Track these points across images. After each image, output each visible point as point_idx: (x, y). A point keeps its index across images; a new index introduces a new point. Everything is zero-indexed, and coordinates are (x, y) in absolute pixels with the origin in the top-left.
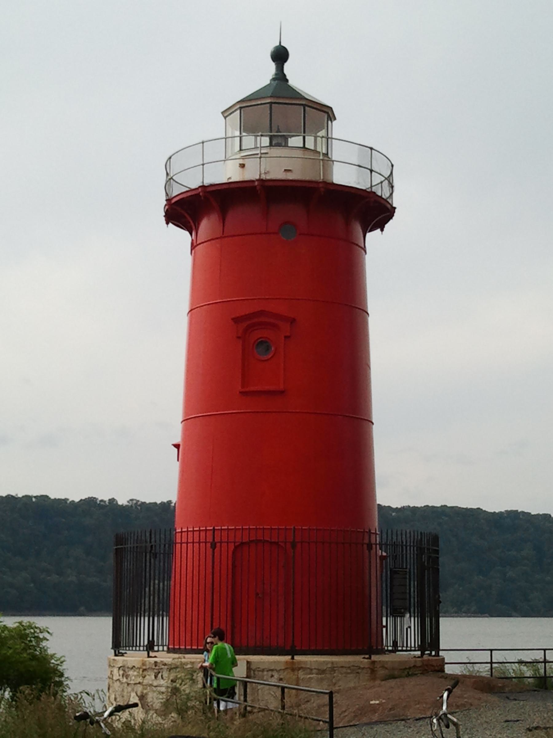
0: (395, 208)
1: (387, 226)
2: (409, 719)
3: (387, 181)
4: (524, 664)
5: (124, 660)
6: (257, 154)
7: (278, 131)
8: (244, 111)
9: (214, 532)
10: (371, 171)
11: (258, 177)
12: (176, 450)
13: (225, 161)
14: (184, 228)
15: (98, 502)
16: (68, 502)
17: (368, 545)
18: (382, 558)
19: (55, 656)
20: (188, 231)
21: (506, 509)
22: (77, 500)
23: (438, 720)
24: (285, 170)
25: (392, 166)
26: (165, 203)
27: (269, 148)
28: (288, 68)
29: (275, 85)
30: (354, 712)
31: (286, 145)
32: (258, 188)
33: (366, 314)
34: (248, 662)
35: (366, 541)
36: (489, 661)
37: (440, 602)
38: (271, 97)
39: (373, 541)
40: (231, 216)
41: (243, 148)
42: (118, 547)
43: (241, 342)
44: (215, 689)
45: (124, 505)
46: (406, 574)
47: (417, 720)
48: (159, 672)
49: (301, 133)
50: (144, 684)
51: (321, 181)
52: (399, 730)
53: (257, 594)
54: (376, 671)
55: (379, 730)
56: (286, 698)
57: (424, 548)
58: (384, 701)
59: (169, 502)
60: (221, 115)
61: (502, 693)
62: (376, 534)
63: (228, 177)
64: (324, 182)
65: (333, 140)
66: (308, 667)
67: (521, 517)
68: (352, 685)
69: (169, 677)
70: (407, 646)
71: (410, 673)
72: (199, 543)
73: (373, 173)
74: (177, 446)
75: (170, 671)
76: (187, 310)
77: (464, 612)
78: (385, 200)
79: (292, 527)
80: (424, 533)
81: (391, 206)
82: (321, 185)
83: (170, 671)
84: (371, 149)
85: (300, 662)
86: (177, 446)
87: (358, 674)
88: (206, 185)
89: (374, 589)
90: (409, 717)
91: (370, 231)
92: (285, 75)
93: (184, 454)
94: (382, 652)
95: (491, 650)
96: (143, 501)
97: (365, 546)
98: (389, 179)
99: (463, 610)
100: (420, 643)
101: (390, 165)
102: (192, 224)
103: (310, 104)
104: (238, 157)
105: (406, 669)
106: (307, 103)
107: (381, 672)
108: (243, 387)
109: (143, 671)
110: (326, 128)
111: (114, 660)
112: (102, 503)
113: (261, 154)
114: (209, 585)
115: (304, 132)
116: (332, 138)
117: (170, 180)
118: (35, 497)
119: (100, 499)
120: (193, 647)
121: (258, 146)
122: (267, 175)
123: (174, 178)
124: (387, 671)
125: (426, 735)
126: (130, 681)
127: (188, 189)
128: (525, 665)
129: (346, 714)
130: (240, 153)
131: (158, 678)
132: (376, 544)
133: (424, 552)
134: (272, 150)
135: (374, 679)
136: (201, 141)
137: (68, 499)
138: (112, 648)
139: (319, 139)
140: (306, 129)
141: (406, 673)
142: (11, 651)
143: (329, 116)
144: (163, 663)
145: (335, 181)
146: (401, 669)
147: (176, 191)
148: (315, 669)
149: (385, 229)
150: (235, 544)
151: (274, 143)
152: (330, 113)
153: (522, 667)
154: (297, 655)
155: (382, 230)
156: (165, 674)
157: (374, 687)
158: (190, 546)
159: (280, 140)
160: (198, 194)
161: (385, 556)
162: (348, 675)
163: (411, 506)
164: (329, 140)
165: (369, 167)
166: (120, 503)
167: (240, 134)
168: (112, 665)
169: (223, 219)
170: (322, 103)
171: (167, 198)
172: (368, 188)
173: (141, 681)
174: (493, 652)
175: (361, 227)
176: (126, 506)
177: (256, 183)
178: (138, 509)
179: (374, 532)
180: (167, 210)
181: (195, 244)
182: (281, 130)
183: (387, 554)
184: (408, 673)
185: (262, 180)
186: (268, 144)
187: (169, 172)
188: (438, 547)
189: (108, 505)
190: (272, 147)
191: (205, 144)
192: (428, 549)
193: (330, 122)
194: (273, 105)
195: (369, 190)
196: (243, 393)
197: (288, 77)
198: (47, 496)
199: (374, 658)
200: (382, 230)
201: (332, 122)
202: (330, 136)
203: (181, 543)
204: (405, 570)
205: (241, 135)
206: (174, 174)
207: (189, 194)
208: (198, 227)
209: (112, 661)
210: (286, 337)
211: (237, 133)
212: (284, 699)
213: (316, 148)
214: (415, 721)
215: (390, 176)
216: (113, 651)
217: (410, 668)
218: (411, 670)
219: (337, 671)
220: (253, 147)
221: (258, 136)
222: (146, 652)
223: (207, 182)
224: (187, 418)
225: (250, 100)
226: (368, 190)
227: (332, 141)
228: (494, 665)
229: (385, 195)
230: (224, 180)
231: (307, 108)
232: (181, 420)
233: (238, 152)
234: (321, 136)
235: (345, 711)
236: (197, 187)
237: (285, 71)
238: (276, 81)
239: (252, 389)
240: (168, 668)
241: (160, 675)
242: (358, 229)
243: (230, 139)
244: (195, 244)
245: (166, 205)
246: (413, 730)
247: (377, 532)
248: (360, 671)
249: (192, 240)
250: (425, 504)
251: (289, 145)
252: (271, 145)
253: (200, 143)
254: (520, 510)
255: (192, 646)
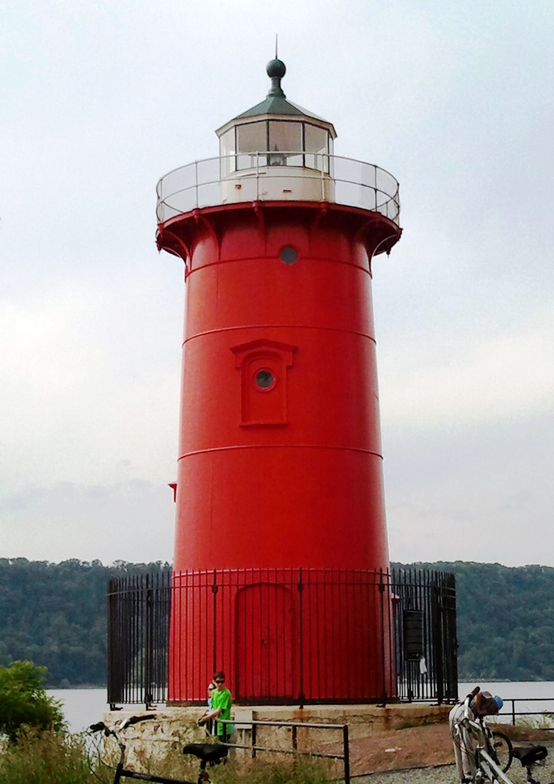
0: (402, 229)
1: (393, 249)
2: (427, 767)
3: (392, 201)
4: (549, 715)
5: (121, 715)
6: (255, 174)
7: (276, 150)
8: (239, 129)
9: (215, 576)
10: (376, 190)
11: (256, 199)
12: (173, 490)
13: (220, 181)
14: (178, 254)
15: (81, 564)
16: (48, 564)
17: (379, 585)
18: (395, 601)
19: (53, 699)
20: (182, 257)
21: (527, 564)
22: (58, 562)
23: (459, 726)
24: (284, 191)
25: (398, 185)
26: (156, 227)
27: (266, 167)
28: (285, 82)
29: (271, 101)
30: (369, 761)
31: (285, 165)
32: (256, 210)
33: (373, 342)
34: (254, 713)
35: (378, 582)
36: (511, 712)
37: (458, 646)
38: (268, 113)
39: (385, 582)
40: (226, 242)
41: (239, 168)
42: (112, 594)
43: (240, 373)
44: (220, 736)
45: (109, 567)
46: (421, 616)
47: (435, 767)
48: (159, 726)
49: (300, 151)
50: (143, 738)
51: (323, 201)
52: (417, 777)
53: (263, 641)
54: (391, 719)
55: (395, 778)
56: (297, 736)
57: (440, 589)
58: (400, 749)
59: (158, 563)
60: (215, 134)
61: (524, 741)
62: (388, 575)
63: (224, 199)
64: (327, 203)
65: (335, 158)
66: (318, 716)
67: (543, 571)
68: (365, 735)
69: (169, 730)
70: (423, 696)
71: (427, 721)
72: (200, 586)
73: (377, 192)
74: (174, 486)
75: (170, 724)
76: (182, 341)
77: (483, 677)
78: (392, 221)
79: (298, 569)
80: (439, 572)
81: (398, 226)
82: (323, 206)
83: (170, 724)
84: (376, 166)
85: (309, 712)
86: (174, 486)
87: (371, 724)
88: (201, 208)
89: (386, 635)
90: (427, 765)
91: (375, 255)
92: (282, 91)
93: (181, 497)
94: (396, 700)
95: (513, 700)
96: (130, 562)
97: (377, 586)
98: (395, 199)
99: (482, 675)
100: (436, 690)
101: (396, 184)
102: (187, 250)
103: (310, 121)
104: (234, 177)
105: (421, 717)
106: (307, 121)
107: (396, 721)
108: (244, 419)
109: (142, 725)
110: (327, 146)
111: (110, 714)
112: (85, 565)
113: (259, 174)
114: (211, 632)
115: (304, 150)
116: (334, 156)
117: (161, 202)
118: (11, 560)
119: (83, 560)
120: (195, 699)
121: (255, 165)
122: (266, 196)
123: (165, 201)
124: (402, 720)
125: (445, 781)
126: (128, 736)
127: (181, 213)
128: (550, 717)
129: (360, 762)
130: (236, 174)
131: (157, 732)
132: (388, 585)
133: (440, 593)
134: (270, 169)
135: (388, 728)
136: (194, 161)
137: (47, 562)
138: (108, 702)
139: (319, 157)
140: (306, 147)
141: (423, 722)
142: (9, 692)
143: (329, 133)
144: (163, 716)
145: (338, 202)
146: (416, 718)
147: (168, 215)
148: (325, 718)
149: (391, 252)
150: (238, 587)
151: (271, 162)
152: (331, 131)
153: (547, 718)
154: (306, 704)
155: (388, 253)
156: (166, 727)
157: (388, 735)
158: (190, 590)
159: (278, 160)
160: (193, 217)
161: (397, 599)
162: (361, 725)
163: (423, 562)
164: (331, 158)
165: (374, 187)
166: (105, 565)
167: (236, 153)
168: (108, 720)
169: (219, 243)
170: (323, 120)
171: (159, 222)
172: (373, 209)
173: (140, 736)
174: (515, 702)
175: (366, 248)
176: (112, 567)
177: (254, 205)
178: (125, 571)
179: (386, 573)
180: (159, 235)
181: (189, 271)
182: (278, 149)
183: (400, 596)
184: (425, 721)
185: (260, 201)
186: (266, 164)
187: (160, 195)
188: (454, 588)
189: (92, 568)
190: (270, 167)
191: (199, 164)
192: (444, 590)
193: (330, 139)
194: (270, 122)
195: (374, 211)
196: (244, 428)
197: (285, 93)
198: (25, 559)
199: (388, 706)
200: (388, 253)
201: (333, 139)
202: (331, 154)
203: (180, 587)
204: (420, 612)
205: (236, 155)
206: (166, 197)
207: (184, 217)
208: (192, 254)
209: (108, 715)
210: (289, 368)
211: (233, 153)
212: (296, 737)
213: (317, 167)
214: (434, 769)
215: (395, 196)
216: (109, 705)
217: (427, 716)
218: (429, 718)
219: (349, 721)
220: (250, 167)
221: (255, 155)
222: (145, 705)
223: (201, 206)
224: (185, 455)
225: (243, 118)
226: (373, 211)
227: (333, 159)
228: (516, 716)
229: (391, 216)
230: (219, 203)
231: (306, 125)
232: (177, 458)
233: (234, 172)
234: (322, 154)
235: (359, 760)
236: (191, 210)
237: (282, 87)
238: (273, 98)
239: (253, 422)
240: (168, 721)
241: (160, 729)
242: (363, 251)
243: (225, 158)
244: (189, 271)
245: (158, 230)
246: (432, 777)
247: (390, 574)
248: (373, 720)
249: (187, 267)
250: (439, 560)
251: (288, 164)
252: (269, 164)
253: (193, 163)
254: (541, 565)
255: (193, 699)
